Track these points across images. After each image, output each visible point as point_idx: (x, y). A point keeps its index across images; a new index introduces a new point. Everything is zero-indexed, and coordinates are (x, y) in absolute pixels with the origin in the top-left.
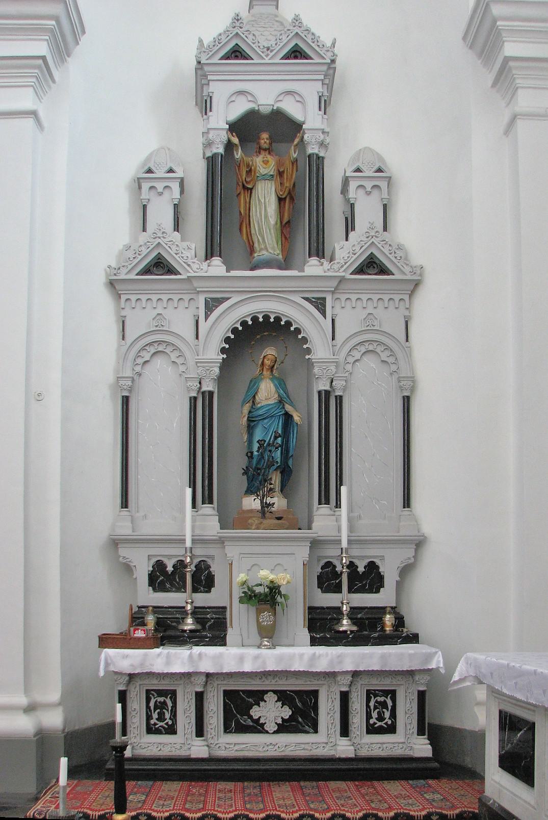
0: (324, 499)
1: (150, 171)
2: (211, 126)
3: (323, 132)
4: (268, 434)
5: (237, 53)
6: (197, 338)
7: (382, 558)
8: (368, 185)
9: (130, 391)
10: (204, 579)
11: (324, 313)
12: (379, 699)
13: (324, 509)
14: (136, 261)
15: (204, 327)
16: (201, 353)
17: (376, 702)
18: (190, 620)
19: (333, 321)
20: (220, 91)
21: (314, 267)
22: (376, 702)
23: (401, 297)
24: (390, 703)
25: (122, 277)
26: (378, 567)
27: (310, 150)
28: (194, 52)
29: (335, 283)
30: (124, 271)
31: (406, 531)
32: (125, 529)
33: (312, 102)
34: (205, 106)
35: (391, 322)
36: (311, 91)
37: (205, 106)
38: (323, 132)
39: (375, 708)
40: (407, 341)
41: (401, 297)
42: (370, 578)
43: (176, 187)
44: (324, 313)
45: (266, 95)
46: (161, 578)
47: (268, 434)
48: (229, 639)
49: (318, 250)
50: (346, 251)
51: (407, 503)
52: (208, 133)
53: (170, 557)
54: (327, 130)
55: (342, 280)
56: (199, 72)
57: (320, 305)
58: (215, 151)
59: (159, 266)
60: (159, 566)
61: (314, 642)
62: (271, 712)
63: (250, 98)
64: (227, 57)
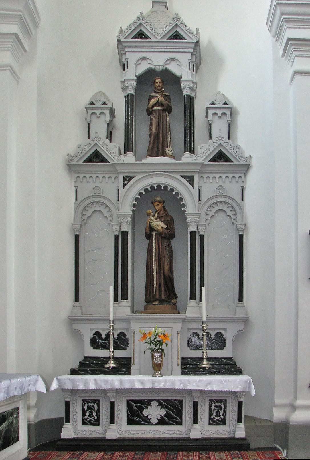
0: (193, 297)
1: (92, 103)
2: (127, 77)
3: (193, 83)
4: (160, 256)
5: (141, 35)
6: (118, 200)
7: (225, 330)
8: (219, 112)
9: (80, 232)
10: (122, 341)
11: (192, 185)
12: (217, 404)
13: (193, 303)
14: (83, 154)
15: (122, 192)
16: (120, 209)
17: (216, 406)
18: (112, 362)
19: (200, 191)
20: (132, 58)
21: (187, 158)
22: (216, 406)
23: (240, 175)
24: (223, 407)
25: (75, 163)
26: (222, 335)
27: (185, 93)
28: (117, 33)
29: (199, 167)
30: (76, 159)
31: (240, 314)
32: (78, 313)
33: (186, 66)
34: (124, 66)
35: (232, 190)
36: (185, 58)
37: (124, 66)
38: (193, 83)
39: (214, 410)
40: (242, 200)
41: (240, 175)
42: (220, 342)
43: (107, 112)
44: (192, 185)
45: (158, 61)
46: (97, 342)
47: (160, 256)
48: (132, 371)
49: (190, 148)
50: (204, 149)
51: (241, 299)
52: (124, 82)
53: (103, 329)
54: (195, 81)
55: (203, 165)
56: (120, 46)
57: (191, 180)
58: (129, 92)
59: (97, 157)
60: (98, 334)
61: (183, 373)
62: (154, 412)
63: (149, 62)
64: (135, 37)
